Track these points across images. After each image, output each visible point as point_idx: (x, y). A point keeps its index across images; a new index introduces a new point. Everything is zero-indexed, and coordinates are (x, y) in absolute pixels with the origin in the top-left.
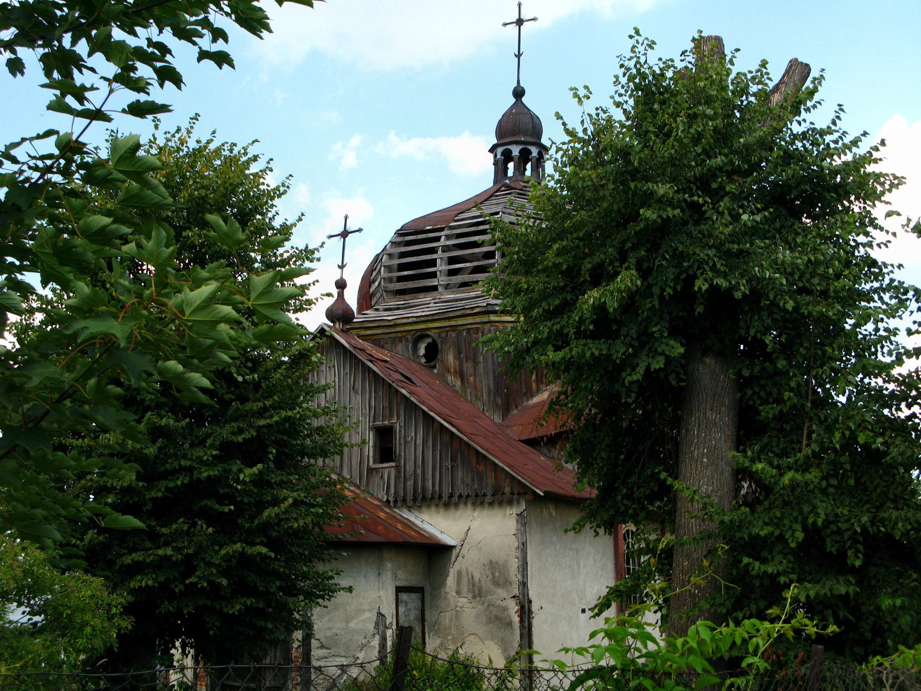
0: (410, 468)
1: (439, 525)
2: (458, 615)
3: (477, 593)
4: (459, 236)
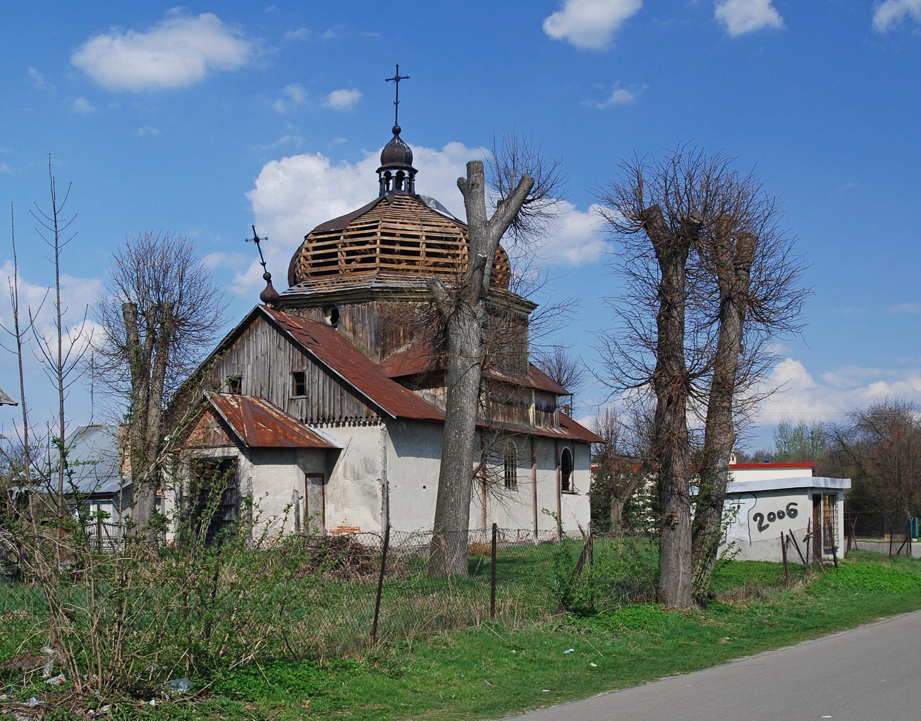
0: (315, 399)
1: (331, 435)
2: (344, 491)
3: (357, 477)
4: (359, 229)
